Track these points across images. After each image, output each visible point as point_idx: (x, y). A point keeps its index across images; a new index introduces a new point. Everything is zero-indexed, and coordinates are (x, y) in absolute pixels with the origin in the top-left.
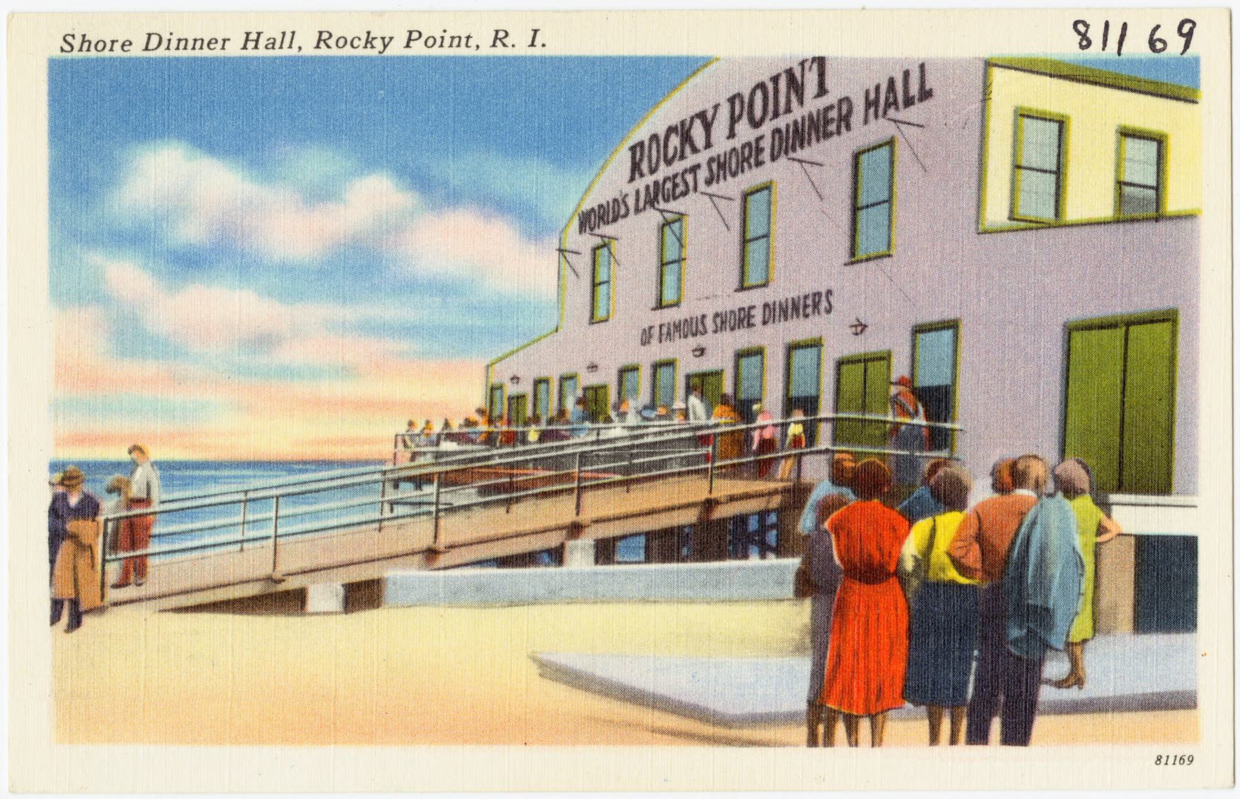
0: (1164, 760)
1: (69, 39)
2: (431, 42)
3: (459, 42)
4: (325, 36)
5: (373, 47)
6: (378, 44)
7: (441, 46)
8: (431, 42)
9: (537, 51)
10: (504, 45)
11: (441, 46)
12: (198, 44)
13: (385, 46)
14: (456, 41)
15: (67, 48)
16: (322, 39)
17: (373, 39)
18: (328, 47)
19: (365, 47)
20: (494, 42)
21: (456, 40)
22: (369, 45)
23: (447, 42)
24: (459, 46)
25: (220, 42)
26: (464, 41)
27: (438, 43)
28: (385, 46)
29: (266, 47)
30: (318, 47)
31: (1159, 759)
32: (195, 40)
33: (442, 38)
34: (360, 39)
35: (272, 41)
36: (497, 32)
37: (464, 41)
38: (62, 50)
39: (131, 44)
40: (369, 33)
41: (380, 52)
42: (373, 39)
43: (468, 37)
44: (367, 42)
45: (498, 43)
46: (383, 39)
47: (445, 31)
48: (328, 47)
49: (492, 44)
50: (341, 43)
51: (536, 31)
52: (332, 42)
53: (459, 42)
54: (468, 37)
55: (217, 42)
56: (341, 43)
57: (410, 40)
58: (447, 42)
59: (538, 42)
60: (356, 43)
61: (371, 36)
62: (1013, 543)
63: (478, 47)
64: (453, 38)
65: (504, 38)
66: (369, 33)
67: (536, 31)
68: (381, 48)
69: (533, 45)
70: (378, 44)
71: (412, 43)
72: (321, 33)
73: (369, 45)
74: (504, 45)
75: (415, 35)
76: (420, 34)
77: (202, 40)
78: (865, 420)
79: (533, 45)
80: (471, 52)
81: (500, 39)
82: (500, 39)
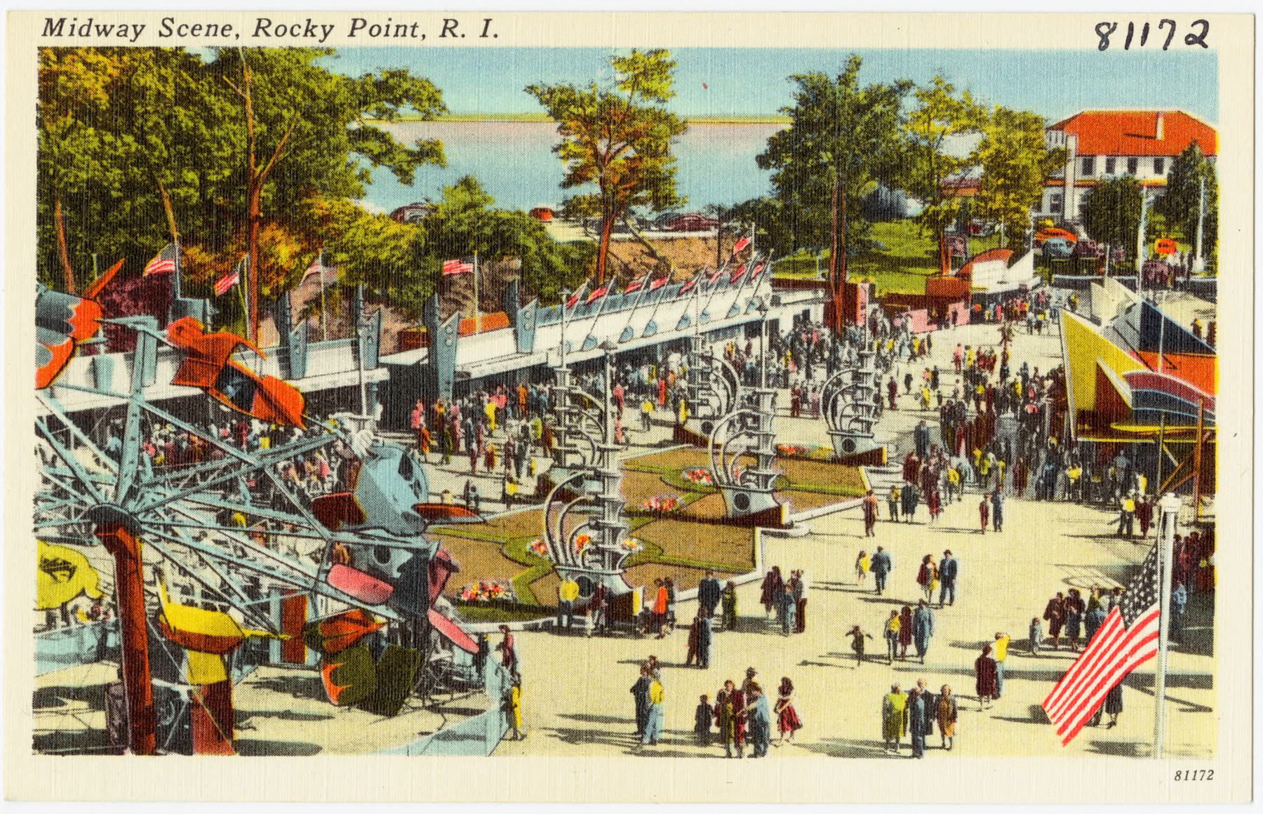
0: (1183, 776)
1: (168, 23)
2: (375, 31)
3: (405, 31)
4: (264, 23)
5: (313, 35)
6: (319, 32)
7: (387, 35)
8: (375, 31)
9: (489, 42)
10: (454, 35)
11: (387, 35)
12: (212, 30)
13: (326, 35)
14: (401, 31)
15: (166, 32)
16: (261, 27)
17: (314, 27)
18: (267, 34)
19: (306, 35)
20: (444, 32)
21: (401, 30)
22: (309, 34)
23: (392, 31)
24: (215, 35)
25: (205, 29)
26: (409, 31)
27: (383, 32)
28: (326, 35)
29: (118, 34)
30: (256, 35)
31: (1178, 775)
32: (209, 26)
33: (388, 26)
34: (187, 27)
35: (124, 28)
36: (447, 21)
37: (409, 31)
38: (161, 34)
39: (231, 29)
40: (309, 21)
41: (320, 41)
42: (314, 27)
43: (414, 27)
44: (307, 30)
45: (261, 32)
46: (324, 27)
47: (390, 19)
48: (267, 34)
49: (441, 33)
50: (281, 31)
51: (488, 21)
52: (271, 30)
53: (405, 31)
54: (414, 27)
55: (201, 29)
56: (281, 31)
57: (354, 28)
58: (392, 31)
59: (490, 32)
60: (296, 31)
61: (311, 24)
62: (394, 438)
63: (424, 36)
64: (398, 27)
65: (267, 27)
66: (309, 21)
67: (488, 21)
68: (322, 37)
69: (484, 35)
70: (319, 32)
71: (356, 32)
72: (355, 20)
73: (309, 34)
74: (454, 35)
75: (359, 24)
76: (365, 23)
77: (216, 26)
78: (542, 373)
79: (484, 35)
80: (417, 42)
81: (263, 28)
82: (263, 28)
